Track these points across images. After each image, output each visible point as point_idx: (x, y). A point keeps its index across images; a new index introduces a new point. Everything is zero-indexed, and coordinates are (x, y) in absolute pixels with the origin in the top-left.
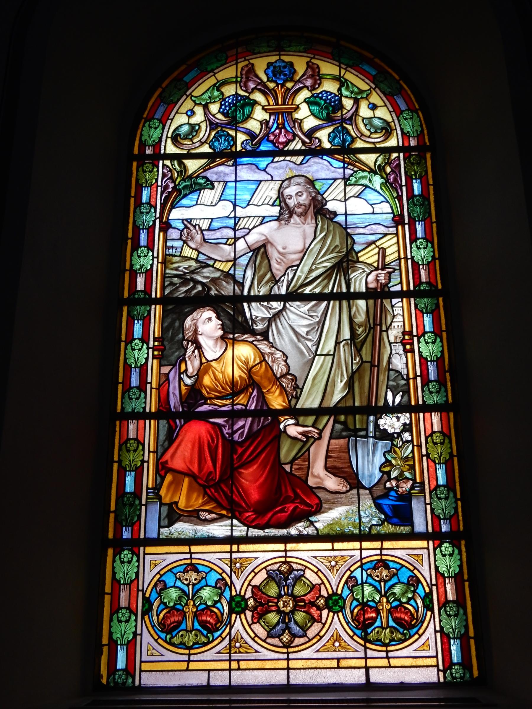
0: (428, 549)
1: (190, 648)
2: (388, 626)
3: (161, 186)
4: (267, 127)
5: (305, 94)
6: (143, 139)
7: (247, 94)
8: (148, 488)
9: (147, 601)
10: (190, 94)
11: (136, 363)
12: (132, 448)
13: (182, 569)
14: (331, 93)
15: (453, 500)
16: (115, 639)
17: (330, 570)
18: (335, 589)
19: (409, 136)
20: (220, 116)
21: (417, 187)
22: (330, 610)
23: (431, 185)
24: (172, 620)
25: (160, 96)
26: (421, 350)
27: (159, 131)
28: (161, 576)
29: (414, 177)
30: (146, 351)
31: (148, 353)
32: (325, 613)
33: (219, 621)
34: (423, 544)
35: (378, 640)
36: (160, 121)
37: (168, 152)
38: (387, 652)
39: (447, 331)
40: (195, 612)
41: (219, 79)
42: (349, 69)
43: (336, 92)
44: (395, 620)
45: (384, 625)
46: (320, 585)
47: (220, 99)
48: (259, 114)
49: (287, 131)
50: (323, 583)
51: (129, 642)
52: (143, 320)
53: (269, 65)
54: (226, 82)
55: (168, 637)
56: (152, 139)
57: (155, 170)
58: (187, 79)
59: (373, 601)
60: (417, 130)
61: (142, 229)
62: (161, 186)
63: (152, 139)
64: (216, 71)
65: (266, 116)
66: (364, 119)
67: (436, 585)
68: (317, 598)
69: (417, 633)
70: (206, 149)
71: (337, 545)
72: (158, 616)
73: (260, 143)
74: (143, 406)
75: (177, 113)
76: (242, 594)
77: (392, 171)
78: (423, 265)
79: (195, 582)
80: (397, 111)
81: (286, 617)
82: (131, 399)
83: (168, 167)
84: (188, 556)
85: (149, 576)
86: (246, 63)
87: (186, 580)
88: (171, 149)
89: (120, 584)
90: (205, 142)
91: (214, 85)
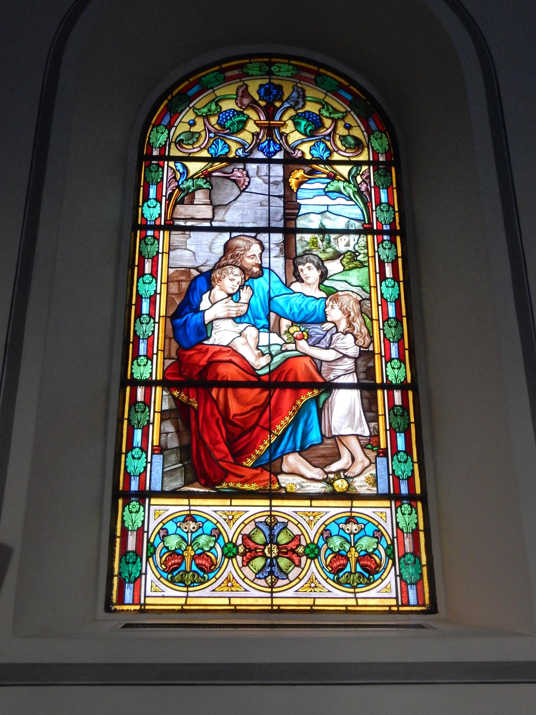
0: (391, 507)
1: (188, 586)
2: (356, 572)
3: (166, 196)
4: (258, 138)
5: (292, 112)
6: (151, 141)
7: (242, 110)
8: (153, 446)
9: (151, 545)
10: (193, 106)
11: (133, 526)
12: (142, 364)
13: (182, 519)
14: (313, 113)
15: (393, 212)
16: (133, 424)
17: (308, 524)
18: (313, 565)
19: (378, 153)
20: (217, 127)
21: (384, 197)
22: (308, 557)
23: (404, 317)
24: (173, 562)
25: (167, 105)
26: (394, 468)
27: (165, 135)
28: (164, 524)
29: (381, 187)
30: (153, 325)
31: (154, 327)
32: (304, 559)
33: (212, 564)
34: (387, 503)
35: (347, 583)
36: (166, 127)
37: (171, 154)
38: (355, 593)
39: (403, 281)
40: (194, 556)
41: (218, 96)
42: (328, 94)
43: (318, 113)
44: (362, 566)
45: (353, 571)
46: (300, 536)
47: (218, 112)
48: (251, 127)
49: (275, 143)
50: (303, 534)
51: (140, 474)
52: (157, 185)
53: (261, 86)
54: (224, 98)
55: (170, 576)
56: (159, 142)
57: (147, 410)
58: (191, 93)
59: (344, 550)
60: (385, 148)
61: (133, 476)
62: (166, 196)
63: (159, 142)
64: (215, 89)
65: (258, 130)
66: (340, 136)
67: (397, 537)
68: (297, 546)
69: (380, 578)
70: (205, 154)
71: (314, 503)
72: (161, 558)
73: (251, 152)
74: (152, 329)
75: (180, 121)
76: (234, 541)
77: (363, 181)
78: (407, 533)
79: (193, 530)
80: (369, 132)
81: (272, 539)
82: (142, 323)
83: (172, 168)
84: (188, 508)
85: (153, 525)
86: (241, 83)
87: (186, 528)
88: (175, 152)
89: (140, 339)
90: (204, 148)
91: (214, 100)
